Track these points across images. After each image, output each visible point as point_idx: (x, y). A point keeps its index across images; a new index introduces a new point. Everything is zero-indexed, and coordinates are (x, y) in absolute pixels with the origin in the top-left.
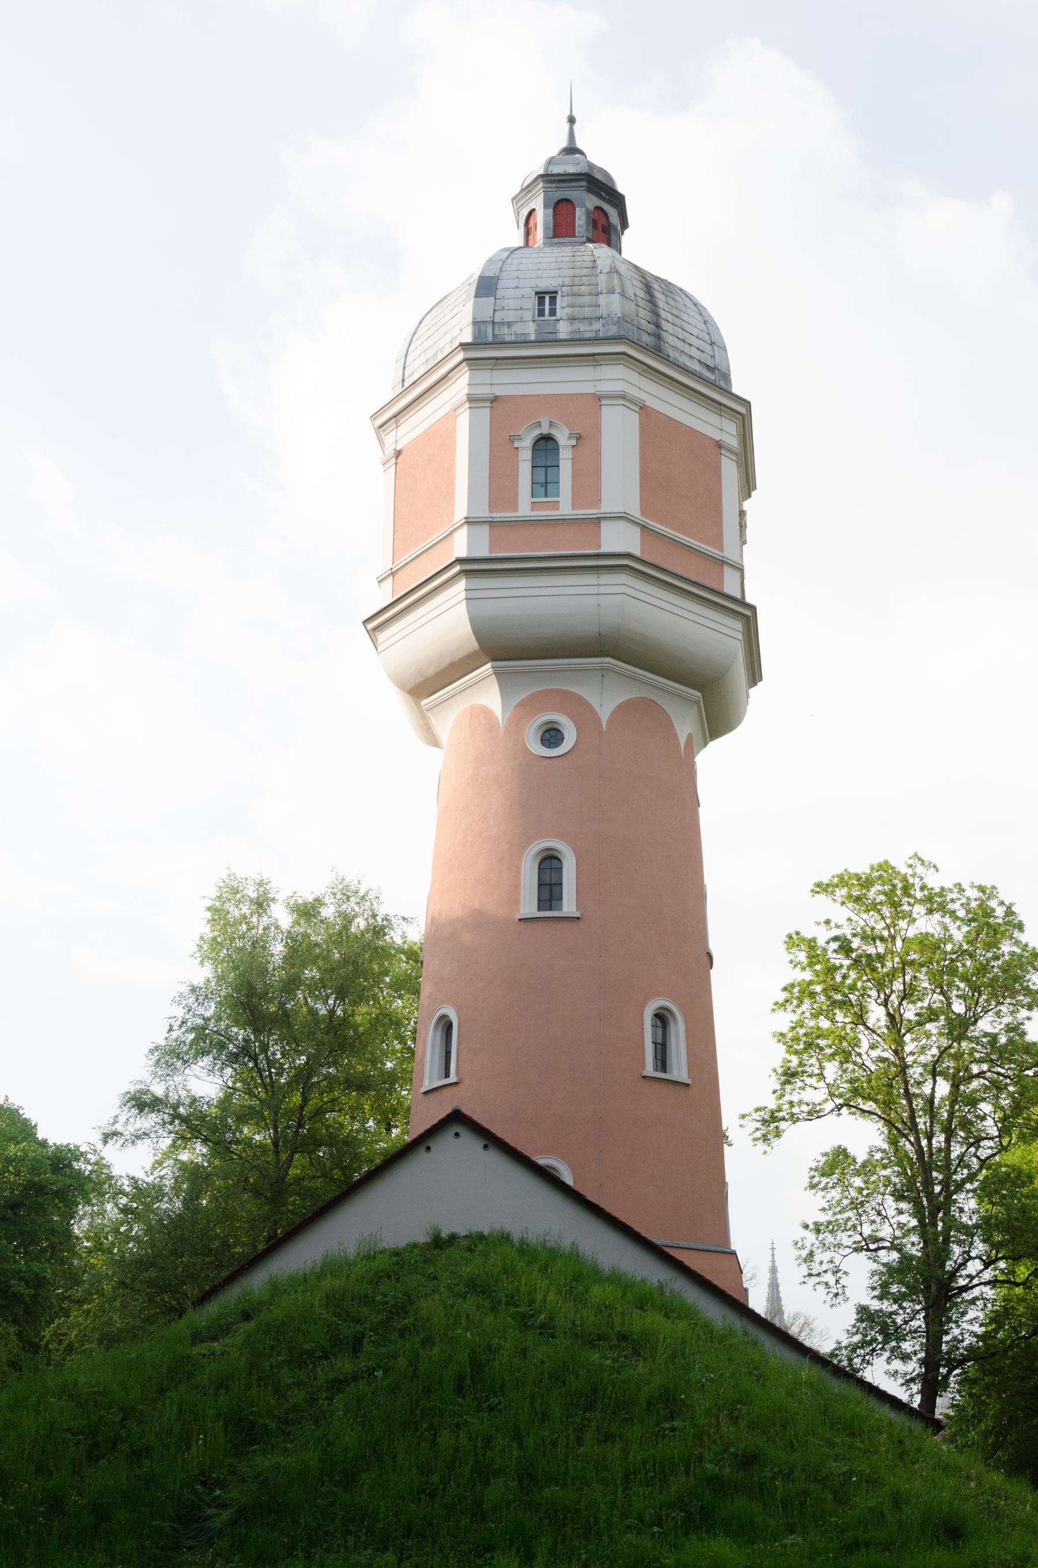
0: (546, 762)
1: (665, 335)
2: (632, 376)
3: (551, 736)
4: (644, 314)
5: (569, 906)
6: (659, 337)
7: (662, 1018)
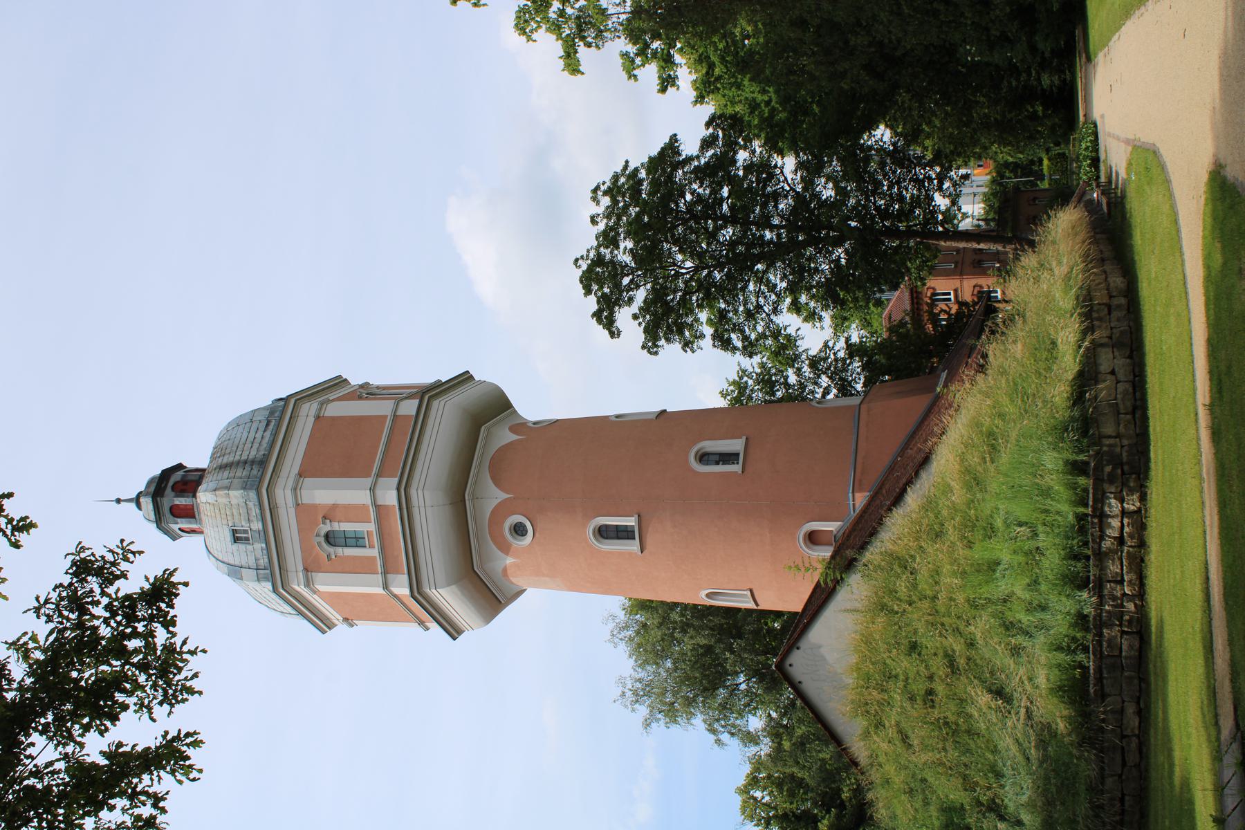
2: (281, 482)
3: (519, 530)
4: (239, 472)
5: (631, 522)
6: (253, 462)
7: (704, 458)
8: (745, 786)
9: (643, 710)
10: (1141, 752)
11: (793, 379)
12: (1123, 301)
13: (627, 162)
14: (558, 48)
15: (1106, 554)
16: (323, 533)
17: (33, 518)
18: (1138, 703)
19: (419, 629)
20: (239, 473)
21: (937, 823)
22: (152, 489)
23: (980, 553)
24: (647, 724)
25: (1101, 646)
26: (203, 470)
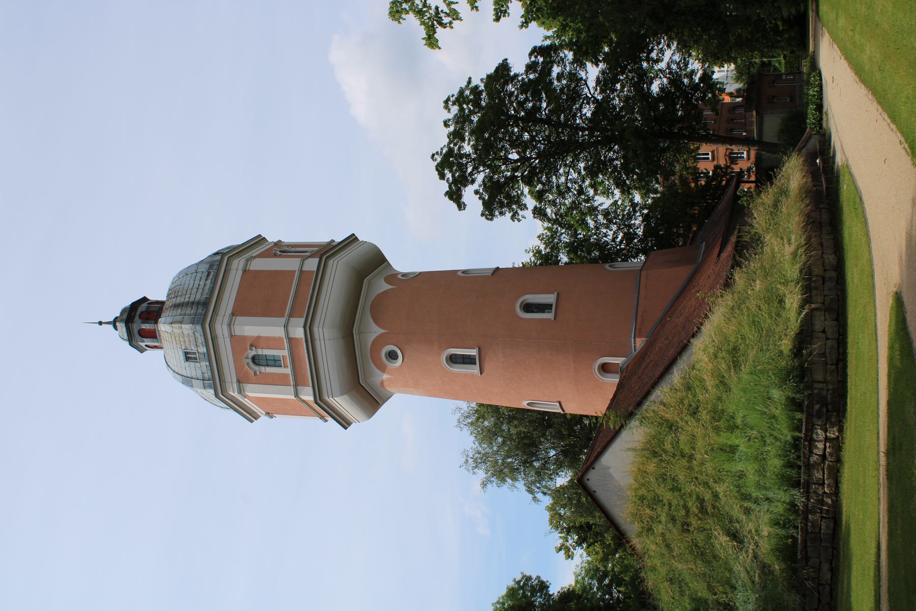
1: (197, 299)
2: (219, 319)
3: (392, 356)
5: (473, 352)
7: (528, 308)
8: (553, 505)
9: (481, 474)
10: (831, 595)
11: (591, 224)
12: (833, 274)
13: (470, 78)
14: (422, 32)
15: (813, 466)
16: (250, 357)
18: (831, 564)
19: (321, 421)
20: (188, 312)
21: (689, 607)
22: (125, 316)
23: (725, 439)
24: (484, 485)
25: (806, 525)
26: (162, 303)
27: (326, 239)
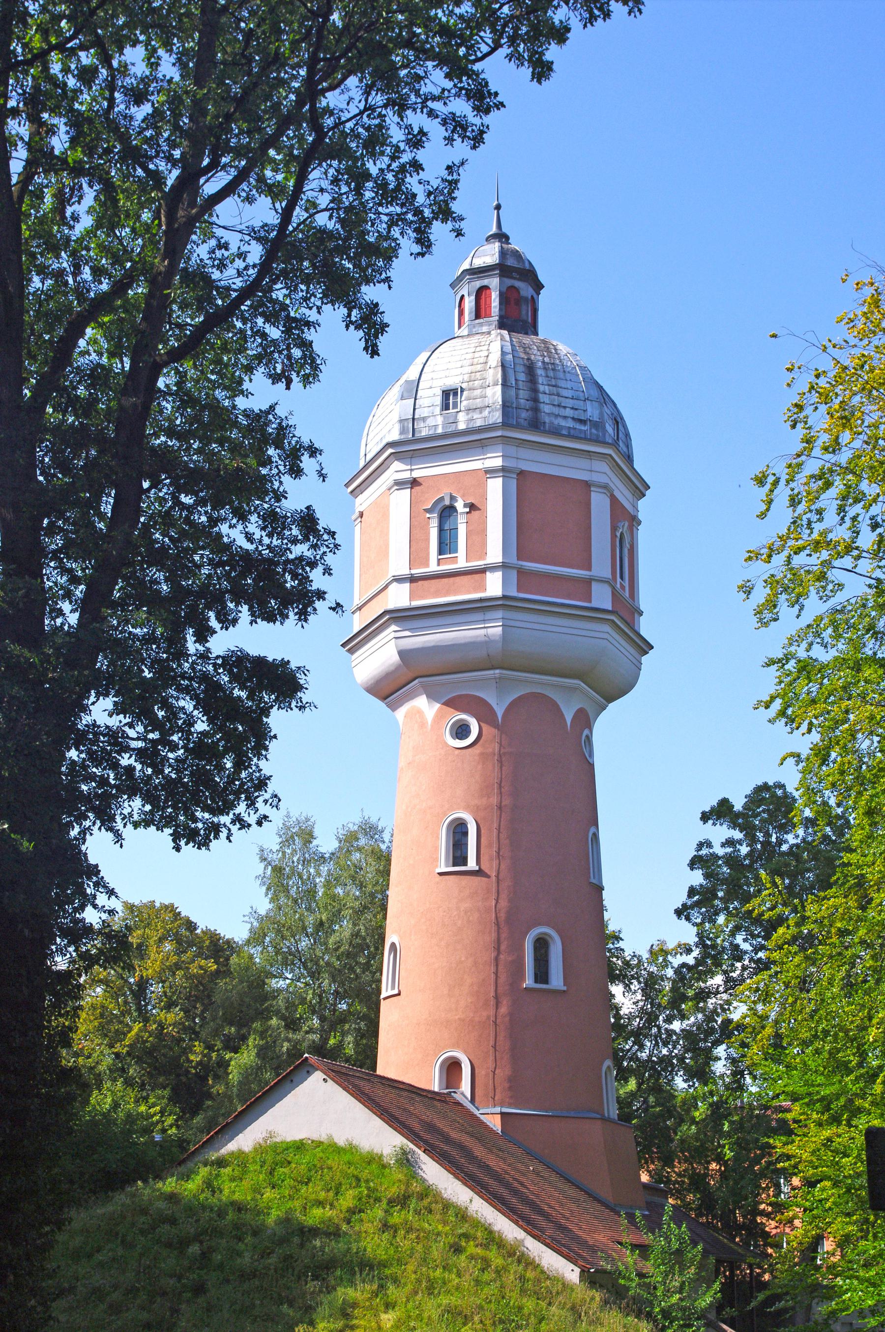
0: (457, 752)
5: (472, 864)
7: (542, 945)
17: (464, 216)
22: (511, 262)
27: (644, 603)
